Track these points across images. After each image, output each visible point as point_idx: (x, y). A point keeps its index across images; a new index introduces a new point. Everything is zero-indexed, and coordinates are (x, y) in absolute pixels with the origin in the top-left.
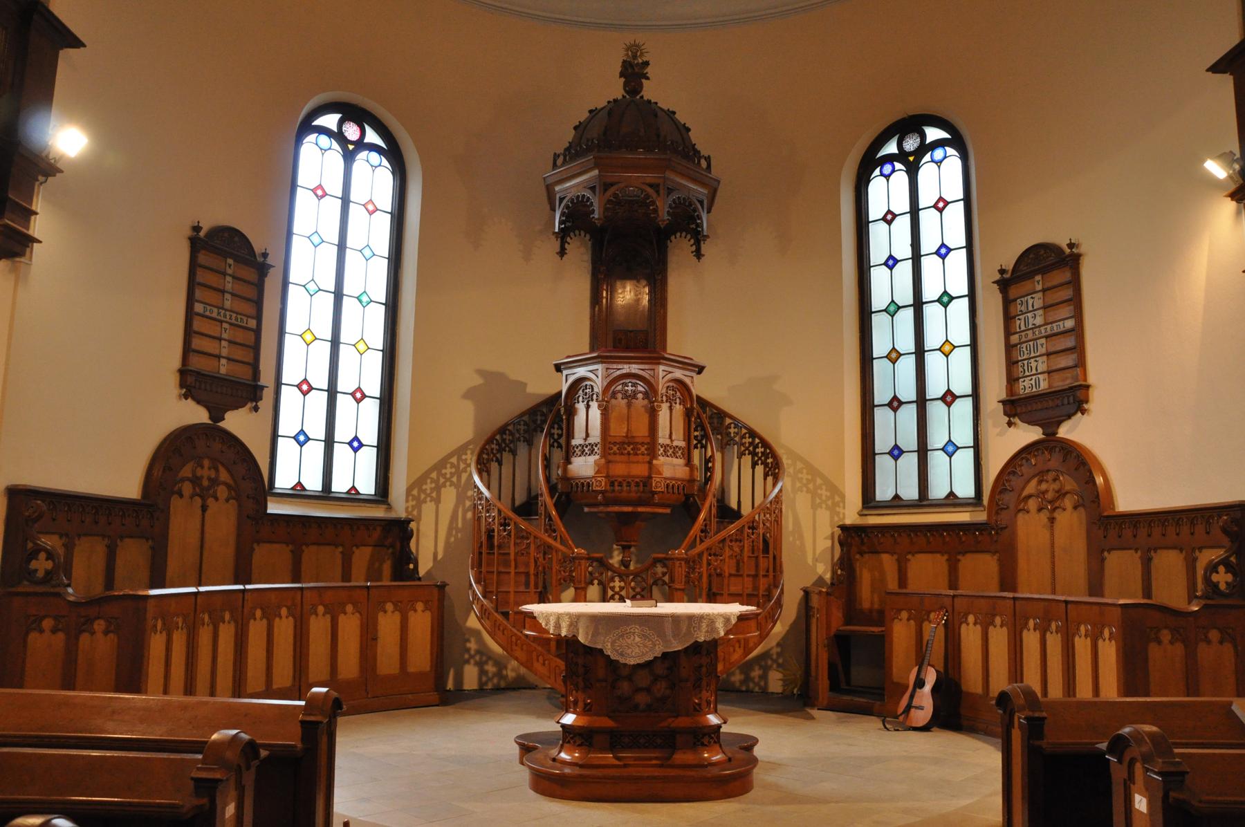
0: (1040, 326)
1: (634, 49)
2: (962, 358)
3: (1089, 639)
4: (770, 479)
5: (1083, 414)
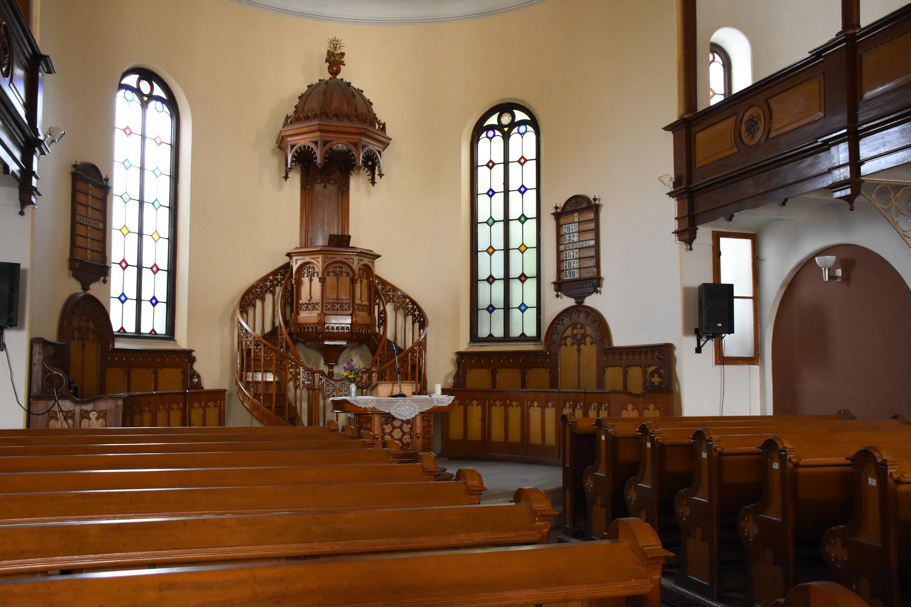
0: (576, 242)
1: (335, 43)
2: (531, 255)
3: (595, 410)
4: (417, 325)
5: (597, 293)
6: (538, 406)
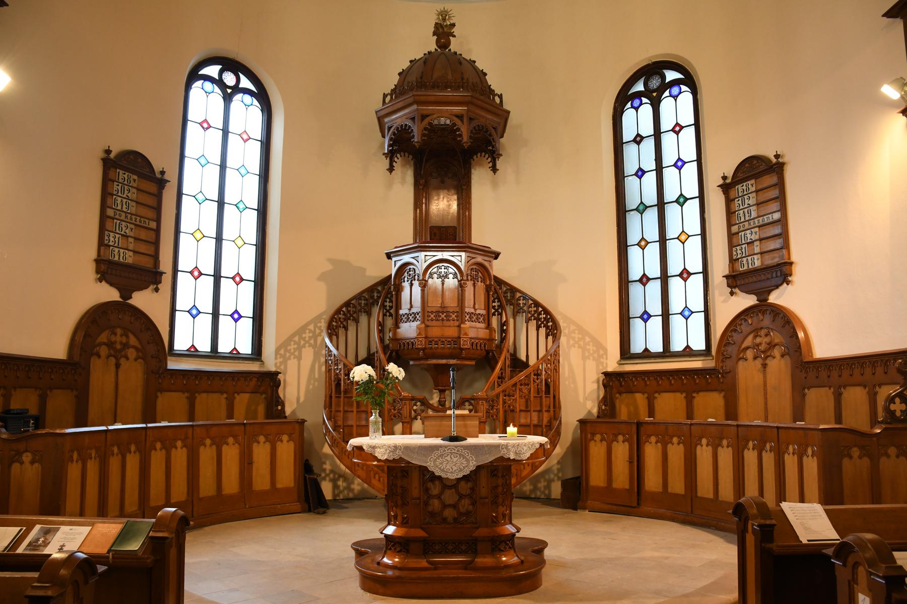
1: (444, 15)
4: (550, 338)
5: (788, 284)
6: (707, 445)
